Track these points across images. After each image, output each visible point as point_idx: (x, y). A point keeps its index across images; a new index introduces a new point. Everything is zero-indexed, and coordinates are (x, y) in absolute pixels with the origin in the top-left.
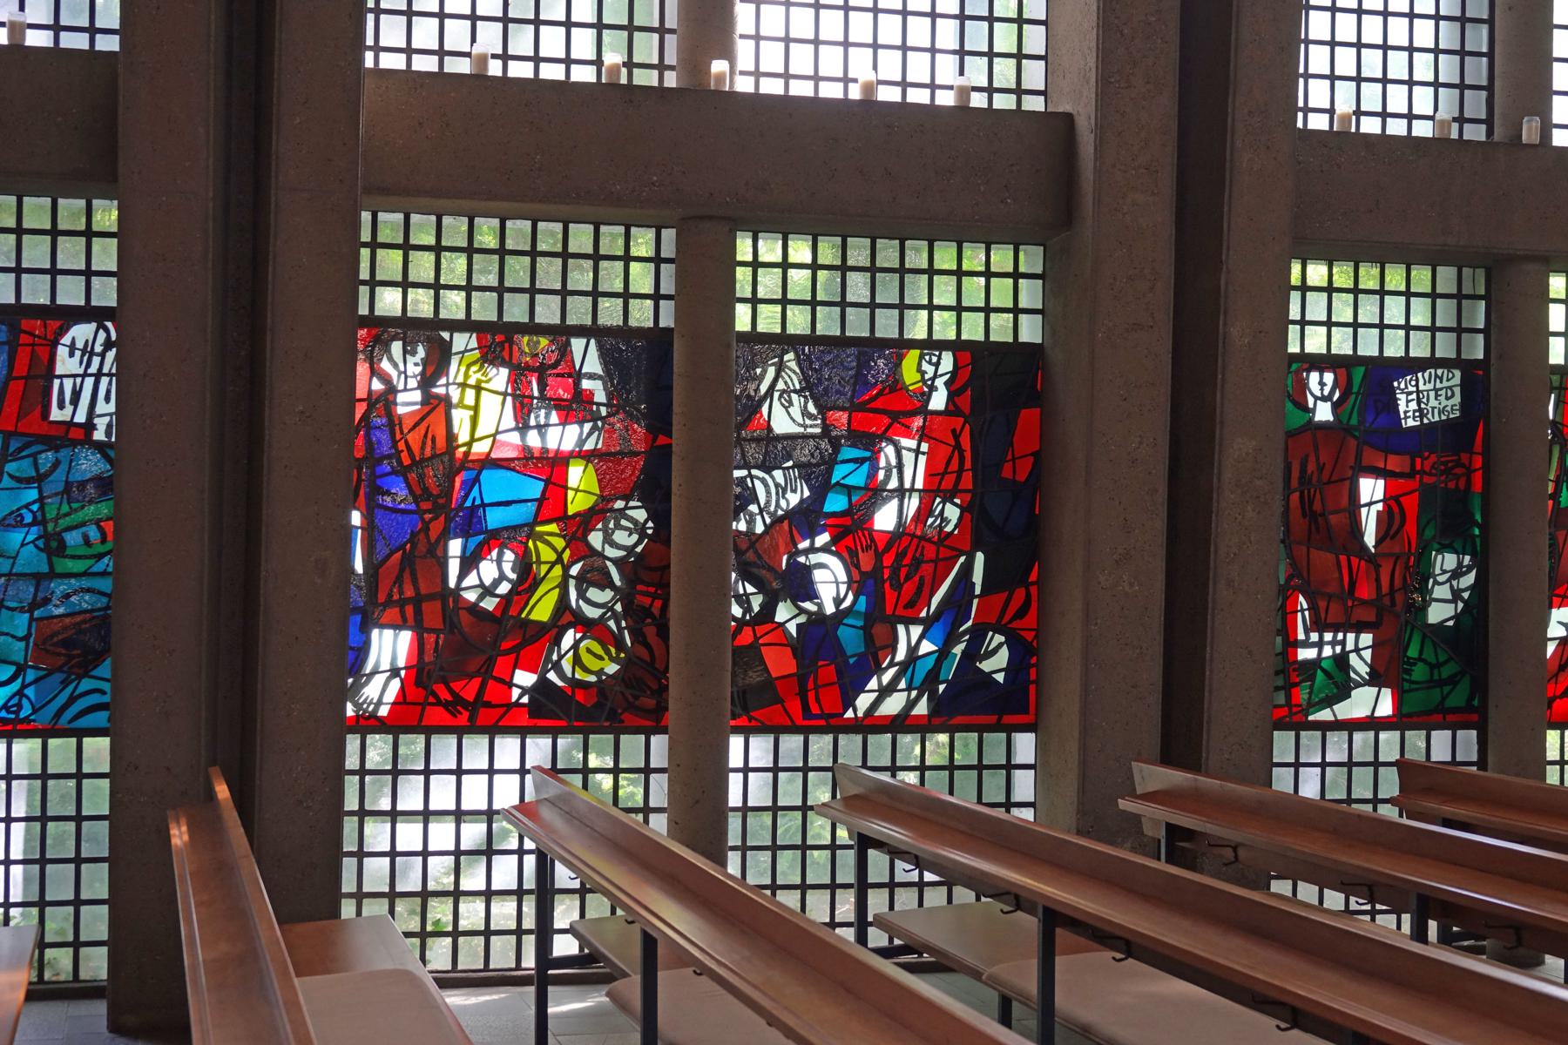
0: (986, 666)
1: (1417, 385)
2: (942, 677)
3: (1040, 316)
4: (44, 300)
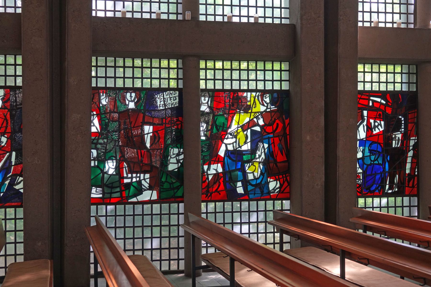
0: (17, 187)
1: (163, 96)
2: (2, 191)
3: (288, 82)
4: (221, 88)
